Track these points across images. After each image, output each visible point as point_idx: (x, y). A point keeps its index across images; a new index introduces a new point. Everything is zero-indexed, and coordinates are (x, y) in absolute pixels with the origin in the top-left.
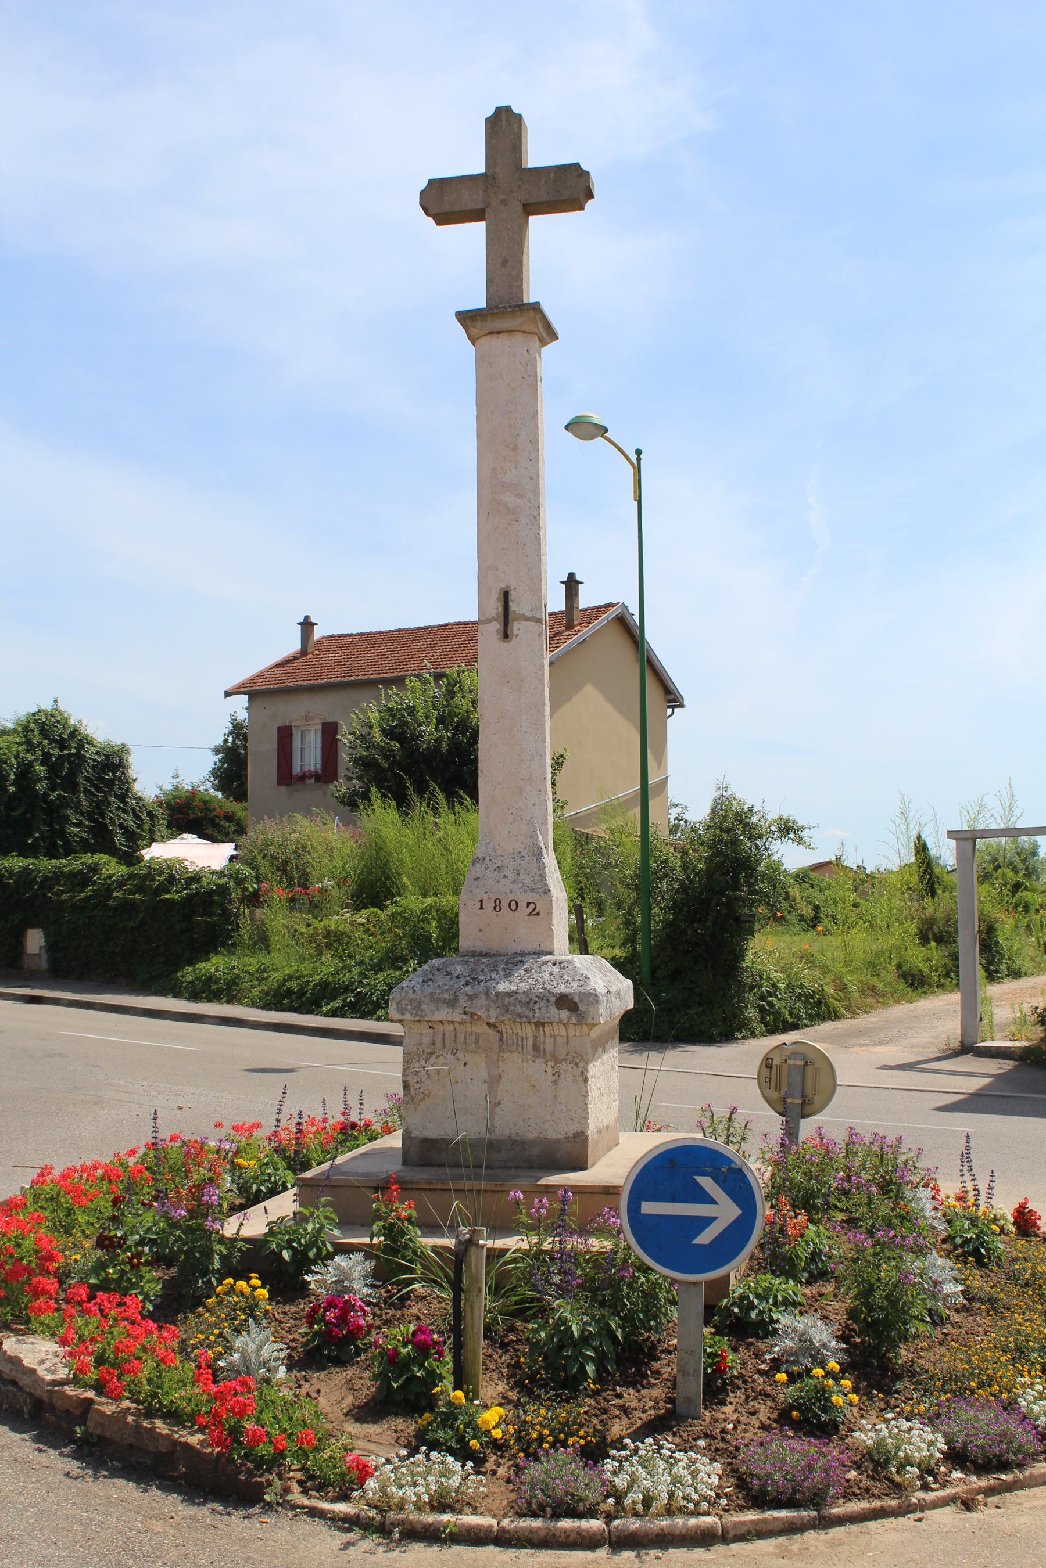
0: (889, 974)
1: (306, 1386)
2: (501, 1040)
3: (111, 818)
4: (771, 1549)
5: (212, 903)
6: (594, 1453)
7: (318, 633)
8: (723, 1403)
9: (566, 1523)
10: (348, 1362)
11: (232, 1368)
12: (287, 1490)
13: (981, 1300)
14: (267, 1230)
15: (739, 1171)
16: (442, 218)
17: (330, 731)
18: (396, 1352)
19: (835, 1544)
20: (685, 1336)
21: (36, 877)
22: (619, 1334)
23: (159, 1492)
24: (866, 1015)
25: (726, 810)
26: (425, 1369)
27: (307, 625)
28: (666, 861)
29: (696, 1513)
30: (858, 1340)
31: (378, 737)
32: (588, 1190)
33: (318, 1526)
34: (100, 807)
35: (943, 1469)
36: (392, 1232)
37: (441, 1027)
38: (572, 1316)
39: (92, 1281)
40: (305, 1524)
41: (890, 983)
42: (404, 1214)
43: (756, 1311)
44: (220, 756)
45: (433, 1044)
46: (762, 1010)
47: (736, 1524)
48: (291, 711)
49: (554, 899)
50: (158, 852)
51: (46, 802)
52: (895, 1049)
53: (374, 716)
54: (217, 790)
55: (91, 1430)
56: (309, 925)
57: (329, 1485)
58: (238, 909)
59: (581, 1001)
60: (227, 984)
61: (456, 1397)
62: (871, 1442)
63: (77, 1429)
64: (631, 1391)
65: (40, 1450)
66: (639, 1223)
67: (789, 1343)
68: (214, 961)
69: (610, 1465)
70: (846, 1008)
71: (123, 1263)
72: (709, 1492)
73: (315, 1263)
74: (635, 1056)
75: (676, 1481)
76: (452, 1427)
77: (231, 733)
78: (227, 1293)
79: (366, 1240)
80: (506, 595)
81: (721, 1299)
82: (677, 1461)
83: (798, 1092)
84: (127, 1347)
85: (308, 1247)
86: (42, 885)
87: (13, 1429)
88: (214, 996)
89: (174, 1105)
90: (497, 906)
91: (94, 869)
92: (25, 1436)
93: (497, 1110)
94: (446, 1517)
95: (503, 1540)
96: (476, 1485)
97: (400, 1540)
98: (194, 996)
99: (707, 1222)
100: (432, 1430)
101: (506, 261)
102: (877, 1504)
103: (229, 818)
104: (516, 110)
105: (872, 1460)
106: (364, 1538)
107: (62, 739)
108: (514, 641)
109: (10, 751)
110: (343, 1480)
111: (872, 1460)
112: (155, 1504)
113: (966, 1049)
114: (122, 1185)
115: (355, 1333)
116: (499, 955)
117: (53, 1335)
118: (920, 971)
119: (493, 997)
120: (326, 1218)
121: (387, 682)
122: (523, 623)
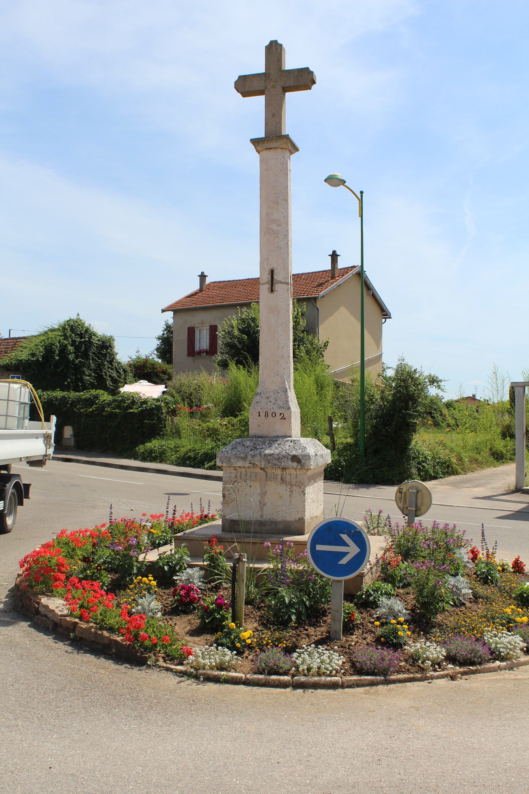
0: (486, 453)
1: (170, 622)
2: (267, 476)
3: (105, 372)
4: (362, 691)
5: (153, 414)
6: (289, 651)
7: (208, 281)
8: (352, 634)
9: (274, 677)
10: (189, 613)
11: (138, 612)
12: (157, 660)
13: (482, 598)
14: (158, 557)
15: (360, 532)
16: (245, 94)
17: (213, 329)
18: (208, 607)
19: (390, 690)
20: (339, 607)
21: (68, 401)
22: (307, 603)
23: (104, 659)
24: (472, 473)
25: (403, 371)
26: (220, 615)
27: (203, 277)
28: (373, 396)
29: (330, 675)
30: (418, 611)
31: (236, 332)
32: (302, 543)
33: (169, 674)
34: (100, 367)
35: (444, 663)
36: (212, 559)
37: (240, 470)
38: (287, 595)
39: (80, 576)
40: (164, 674)
41: (485, 457)
42: (218, 551)
43: (372, 597)
44: (160, 341)
45: (236, 477)
46: (419, 470)
47: (348, 680)
48: (194, 320)
49: (292, 412)
50: (127, 389)
51: (73, 364)
52: (483, 489)
53: (235, 323)
54: (159, 358)
55: (77, 635)
56: (200, 425)
57: (175, 659)
58: (166, 417)
59: (303, 458)
60: (160, 454)
61: (232, 626)
62: (412, 650)
63: (71, 634)
64: (312, 628)
65: (56, 642)
66: (315, 554)
67: (384, 610)
68: (153, 442)
69: (295, 655)
70: (462, 469)
71: (94, 569)
72: (337, 667)
73: (178, 571)
74: (355, 490)
75: (322, 662)
76: (229, 638)
77: (165, 330)
78: (139, 583)
79: (202, 563)
80: (272, 272)
81: (358, 592)
82: (324, 654)
83: (414, 505)
84: (92, 601)
85: (176, 565)
86: (71, 404)
87: (45, 634)
88: (153, 460)
89: (129, 508)
90: (266, 415)
91: (96, 397)
92: (50, 637)
93: (264, 507)
94: (223, 673)
95: (247, 683)
96: (238, 661)
97: (203, 681)
98: (144, 459)
99: (345, 554)
100: (221, 639)
101: (274, 115)
102: (412, 675)
103: (164, 372)
104: (279, 42)
105: (413, 658)
106: (188, 679)
107: (81, 333)
108: (276, 293)
109: (56, 339)
110: (181, 657)
111: (413, 658)
112: (102, 664)
113: (518, 490)
114: (97, 539)
115: (193, 600)
116: (267, 437)
117: (63, 597)
118: (501, 452)
119: (263, 456)
120: (184, 552)
121: (242, 305)
122: (280, 285)
